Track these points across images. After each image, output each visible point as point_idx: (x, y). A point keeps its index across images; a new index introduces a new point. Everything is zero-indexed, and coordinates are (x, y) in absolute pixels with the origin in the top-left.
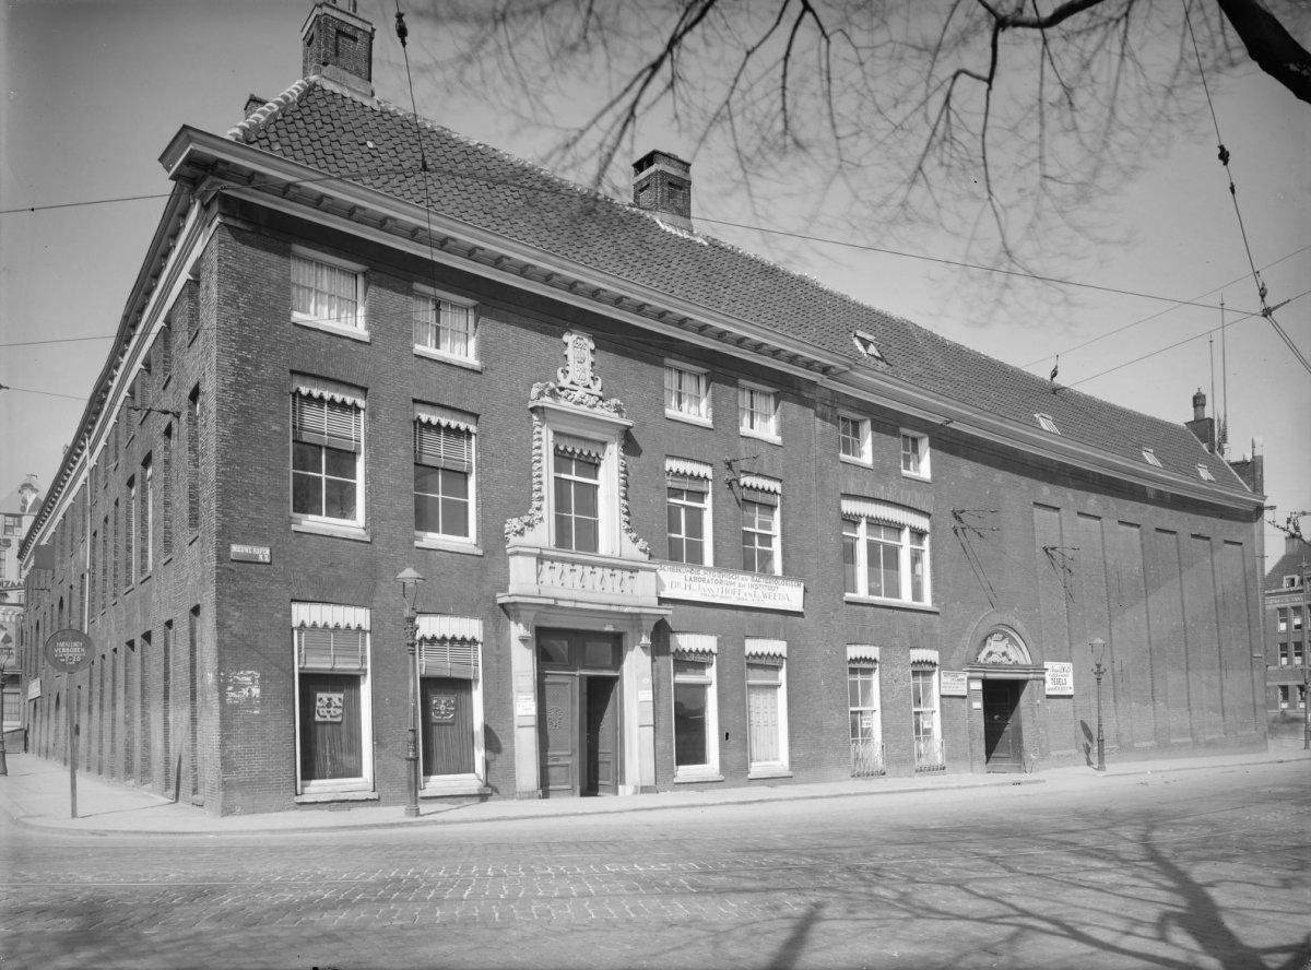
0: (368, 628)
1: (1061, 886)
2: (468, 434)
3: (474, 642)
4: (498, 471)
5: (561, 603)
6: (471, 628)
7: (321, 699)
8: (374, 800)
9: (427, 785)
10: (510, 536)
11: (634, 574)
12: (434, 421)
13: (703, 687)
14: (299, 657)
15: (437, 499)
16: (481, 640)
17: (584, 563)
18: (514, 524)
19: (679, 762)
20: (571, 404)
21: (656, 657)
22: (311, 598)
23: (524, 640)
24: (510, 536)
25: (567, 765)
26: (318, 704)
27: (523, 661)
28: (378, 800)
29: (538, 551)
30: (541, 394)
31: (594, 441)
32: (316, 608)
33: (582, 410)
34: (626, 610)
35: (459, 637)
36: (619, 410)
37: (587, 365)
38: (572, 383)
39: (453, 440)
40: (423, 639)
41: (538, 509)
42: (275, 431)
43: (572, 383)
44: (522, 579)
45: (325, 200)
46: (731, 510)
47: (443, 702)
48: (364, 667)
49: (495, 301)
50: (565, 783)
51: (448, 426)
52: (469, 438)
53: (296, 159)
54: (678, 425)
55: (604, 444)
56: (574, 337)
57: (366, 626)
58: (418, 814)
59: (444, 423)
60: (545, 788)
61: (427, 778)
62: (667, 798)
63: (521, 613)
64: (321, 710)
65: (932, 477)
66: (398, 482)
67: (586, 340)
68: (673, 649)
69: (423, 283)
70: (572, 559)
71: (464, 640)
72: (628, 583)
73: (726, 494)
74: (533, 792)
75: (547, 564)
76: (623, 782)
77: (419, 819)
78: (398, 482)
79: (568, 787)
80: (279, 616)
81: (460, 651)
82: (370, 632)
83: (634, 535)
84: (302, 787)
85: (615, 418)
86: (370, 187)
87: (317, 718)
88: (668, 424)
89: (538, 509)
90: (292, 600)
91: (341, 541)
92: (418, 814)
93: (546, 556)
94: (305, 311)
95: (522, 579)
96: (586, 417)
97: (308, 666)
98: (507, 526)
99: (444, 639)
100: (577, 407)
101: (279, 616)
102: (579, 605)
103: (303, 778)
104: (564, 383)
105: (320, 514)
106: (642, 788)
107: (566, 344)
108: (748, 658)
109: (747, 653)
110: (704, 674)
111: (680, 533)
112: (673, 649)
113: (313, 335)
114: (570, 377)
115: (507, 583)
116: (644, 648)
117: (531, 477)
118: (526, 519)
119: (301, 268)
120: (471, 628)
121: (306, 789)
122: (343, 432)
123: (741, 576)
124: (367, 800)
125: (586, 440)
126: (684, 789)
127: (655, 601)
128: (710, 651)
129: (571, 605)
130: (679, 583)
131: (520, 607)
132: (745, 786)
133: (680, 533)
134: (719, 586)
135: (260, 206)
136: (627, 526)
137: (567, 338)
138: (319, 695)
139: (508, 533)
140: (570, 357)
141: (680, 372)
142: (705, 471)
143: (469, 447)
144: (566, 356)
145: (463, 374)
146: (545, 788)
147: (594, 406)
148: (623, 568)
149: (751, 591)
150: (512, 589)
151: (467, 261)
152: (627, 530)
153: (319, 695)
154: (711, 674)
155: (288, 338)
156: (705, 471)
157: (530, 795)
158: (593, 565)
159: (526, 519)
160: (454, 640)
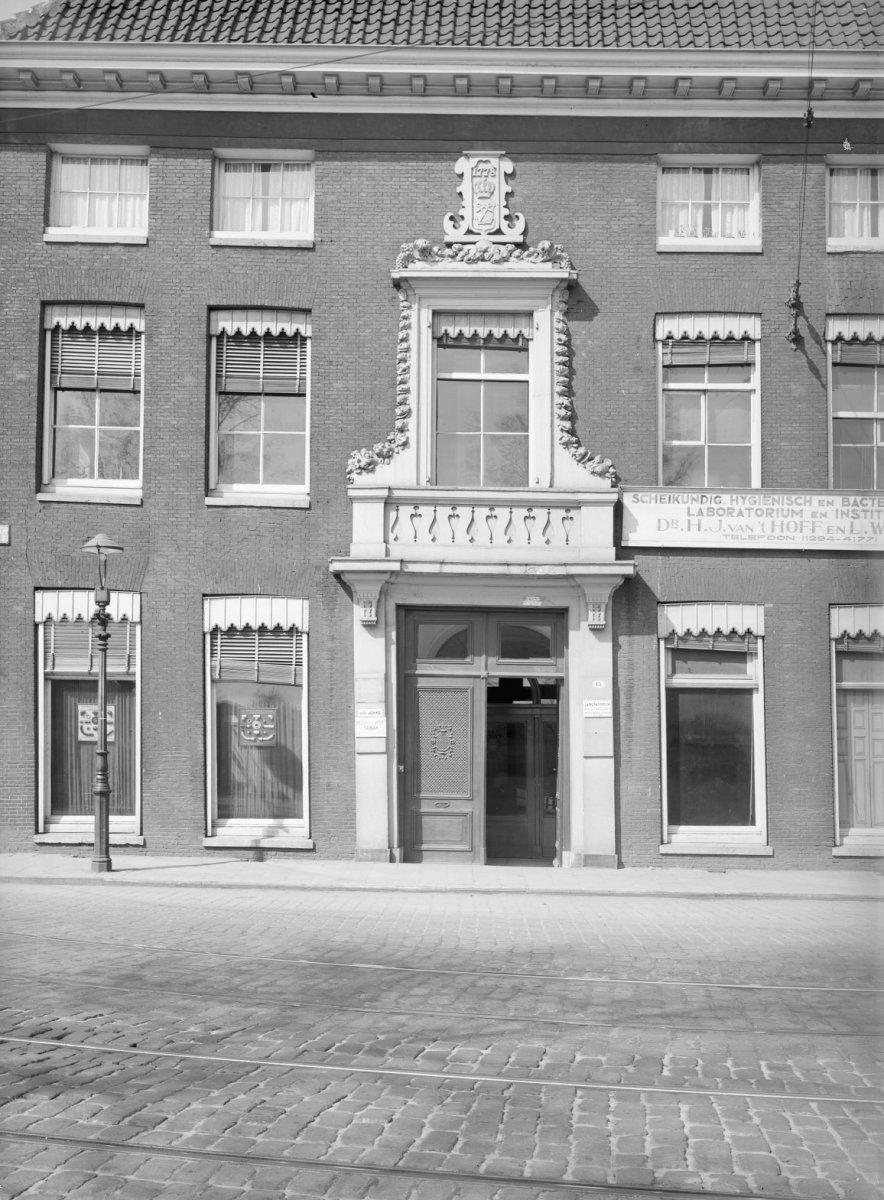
0: (137, 619)
1: (269, 1155)
2: (298, 339)
3: (293, 630)
4: (339, 385)
5: (412, 568)
6: (291, 612)
7: (83, 713)
8: (137, 846)
9: (219, 831)
10: (354, 476)
11: (573, 513)
12: (80, 325)
13: (748, 692)
14: (45, 659)
15: (259, 430)
16: (762, 632)
17: (512, 504)
18: (361, 457)
19: (676, 818)
20: (463, 266)
21: (623, 640)
22: (60, 584)
23: (369, 626)
24: (354, 476)
25: (465, 815)
26: (80, 718)
27: (371, 658)
28: (313, 850)
29: (385, 493)
30: (409, 259)
31: (514, 314)
32: (65, 597)
33: (485, 269)
34: (540, 571)
35: (270, 626)
36: (551, 257)
37: (498, 199)
38: (469, 232)
39: (277, 351)
40: (215, 631)
41: (402, 430)
42: (20, 381)
43: (469, 232)
44: (367, 537)
45: (772, 85)
46: (800, 386)
47: (257, 716)
48: (132, 670)
49: (333, 138)
50: (461, 842)
51: (268, 334)
52: (303, 344)
53: (769, 46)
54: (682, 260)
55: (530, 314)
56: (473, 161)
57: (759, 629)
58: (109, 868)
59: (95, 326)
60: (410, 844)
61: (673, 827)
62: (632, 878)
63: (588, 591)
64: (85, 726)
65: (765, 242)
66: (183, 421)
67: (495, 162)
68: (663, 631)
69: (229, 146)
70: (507, 501)
71: (278, 629)
72: (557, 530)
73: (791, 359)
74: (380, 851)
75: (406, 511)
76: (569, 849)
77: (107, 876)
78: (183, 421)
79: (467, 847)
80: (20, 608)
81: (276, 647)
82: (763, 637)
83: (582, 450)
84: (842, 836)
85: (547, 271)
86: (844, 48)
87: (81, 737)
88: (662, 261)
89: (402, 430)
90: (36, 589)
91: (100, 508)
92: (109, 868)
93: (399, 499)
94: (841, 235)
95: (367, 537)
96: (437, 279)
97: (57, 670)
98: (350, 461)
99: (247, 629)
100: (474, 266)
101: (20, 608)
102: (447, 569)
103: (671, 822)
104: (453, 234)
105: (255, 481)
106: (587, 857)
107: (461, 176)
108: (838, 641)
109: (835, 633)
110: (744, 672)
111: (699, 439)
112: (663, 631)
113: (72, 252)
114: (464, 226)
115: (348, 539)
116: (596, 630)
117: (394, 385)
118: (378, 447)
119: (675, 182)
120: (291, 612)
121: (674, 836)
122: (119, 367)
123: (816, 499)
124: (127, 845)
125: (499, 314)
126: (683, 865)
127: (610, 552)
128: (749, 632)
129: (435, 569)
130: (658, 519)
131: (579, 581)
132: (826, 867)
133: (699, 439)
134: (767, 521)
135: (290, 113)
136: (567, 437)
137: (463, 165)
138: (81, 708)
139: (350, 472)
140: (467, 195)
141: (874, 172)
142: (752, 326)
143: (303, 353)
144: (460, 194)
145: (283, 256)
146: (410, 844)
147: (505, 260)
148: (549, 506)
149: (845, 523)
150: (356, 550)
151: (541, 100)
152: (567, 445)
153: (81, 708)
154: (753, 673)
155: (41, 262)
156: (752, 326)
157: (373, 856)
158: (530, 505)
159: (378, 447)
160: (262, 629)
